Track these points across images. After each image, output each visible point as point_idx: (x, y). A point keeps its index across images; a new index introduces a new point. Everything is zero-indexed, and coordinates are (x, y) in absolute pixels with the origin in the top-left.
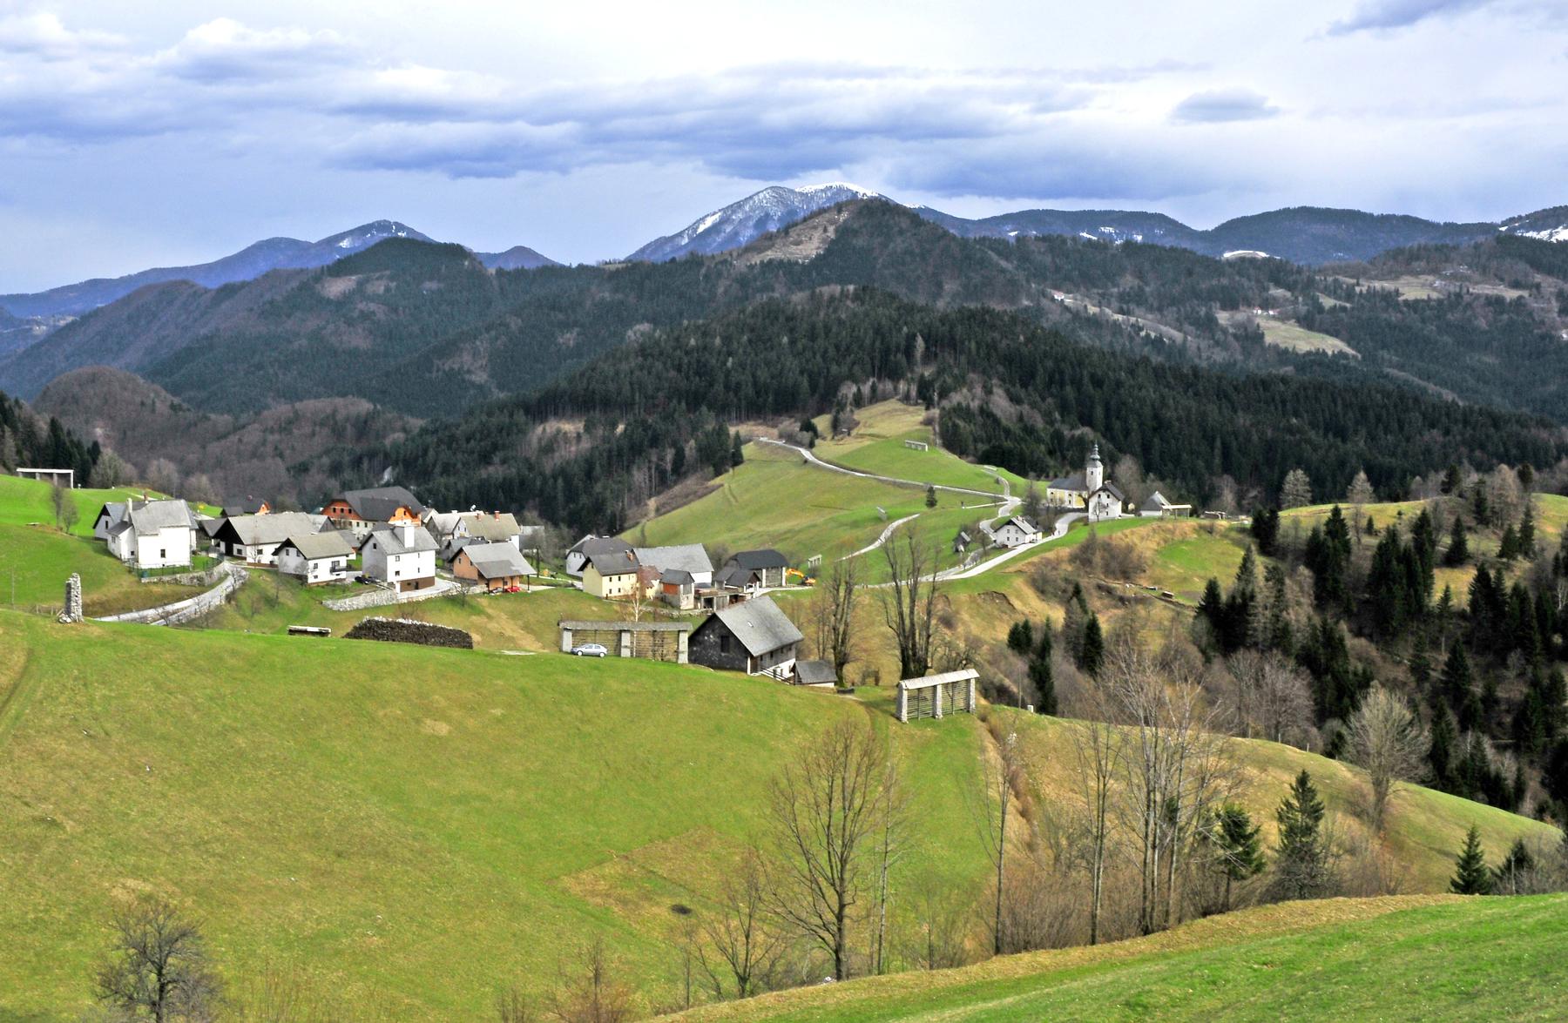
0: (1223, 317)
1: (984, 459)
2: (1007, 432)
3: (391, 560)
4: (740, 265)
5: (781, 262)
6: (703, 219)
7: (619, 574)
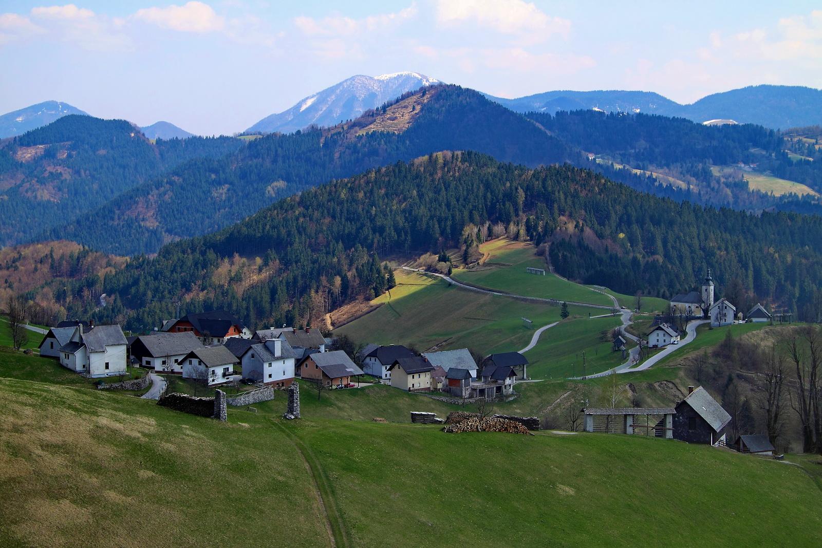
0: (715, 171)
1: (588, 281)
2: (601, 261)
3: (266, 365)
4: (352, 136)
5: (382, 133)
6: (304, 101)
7: (419, 372)
